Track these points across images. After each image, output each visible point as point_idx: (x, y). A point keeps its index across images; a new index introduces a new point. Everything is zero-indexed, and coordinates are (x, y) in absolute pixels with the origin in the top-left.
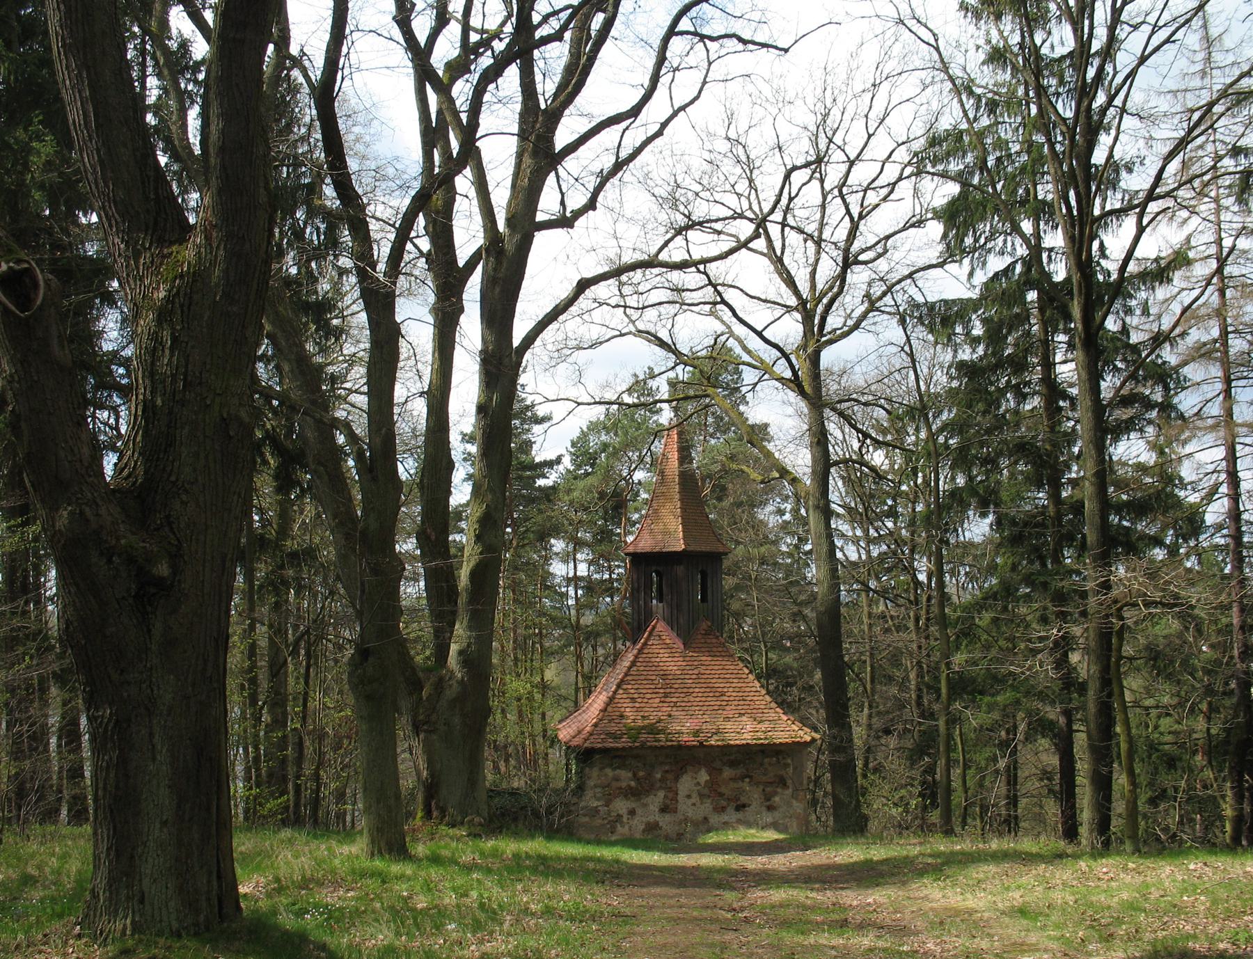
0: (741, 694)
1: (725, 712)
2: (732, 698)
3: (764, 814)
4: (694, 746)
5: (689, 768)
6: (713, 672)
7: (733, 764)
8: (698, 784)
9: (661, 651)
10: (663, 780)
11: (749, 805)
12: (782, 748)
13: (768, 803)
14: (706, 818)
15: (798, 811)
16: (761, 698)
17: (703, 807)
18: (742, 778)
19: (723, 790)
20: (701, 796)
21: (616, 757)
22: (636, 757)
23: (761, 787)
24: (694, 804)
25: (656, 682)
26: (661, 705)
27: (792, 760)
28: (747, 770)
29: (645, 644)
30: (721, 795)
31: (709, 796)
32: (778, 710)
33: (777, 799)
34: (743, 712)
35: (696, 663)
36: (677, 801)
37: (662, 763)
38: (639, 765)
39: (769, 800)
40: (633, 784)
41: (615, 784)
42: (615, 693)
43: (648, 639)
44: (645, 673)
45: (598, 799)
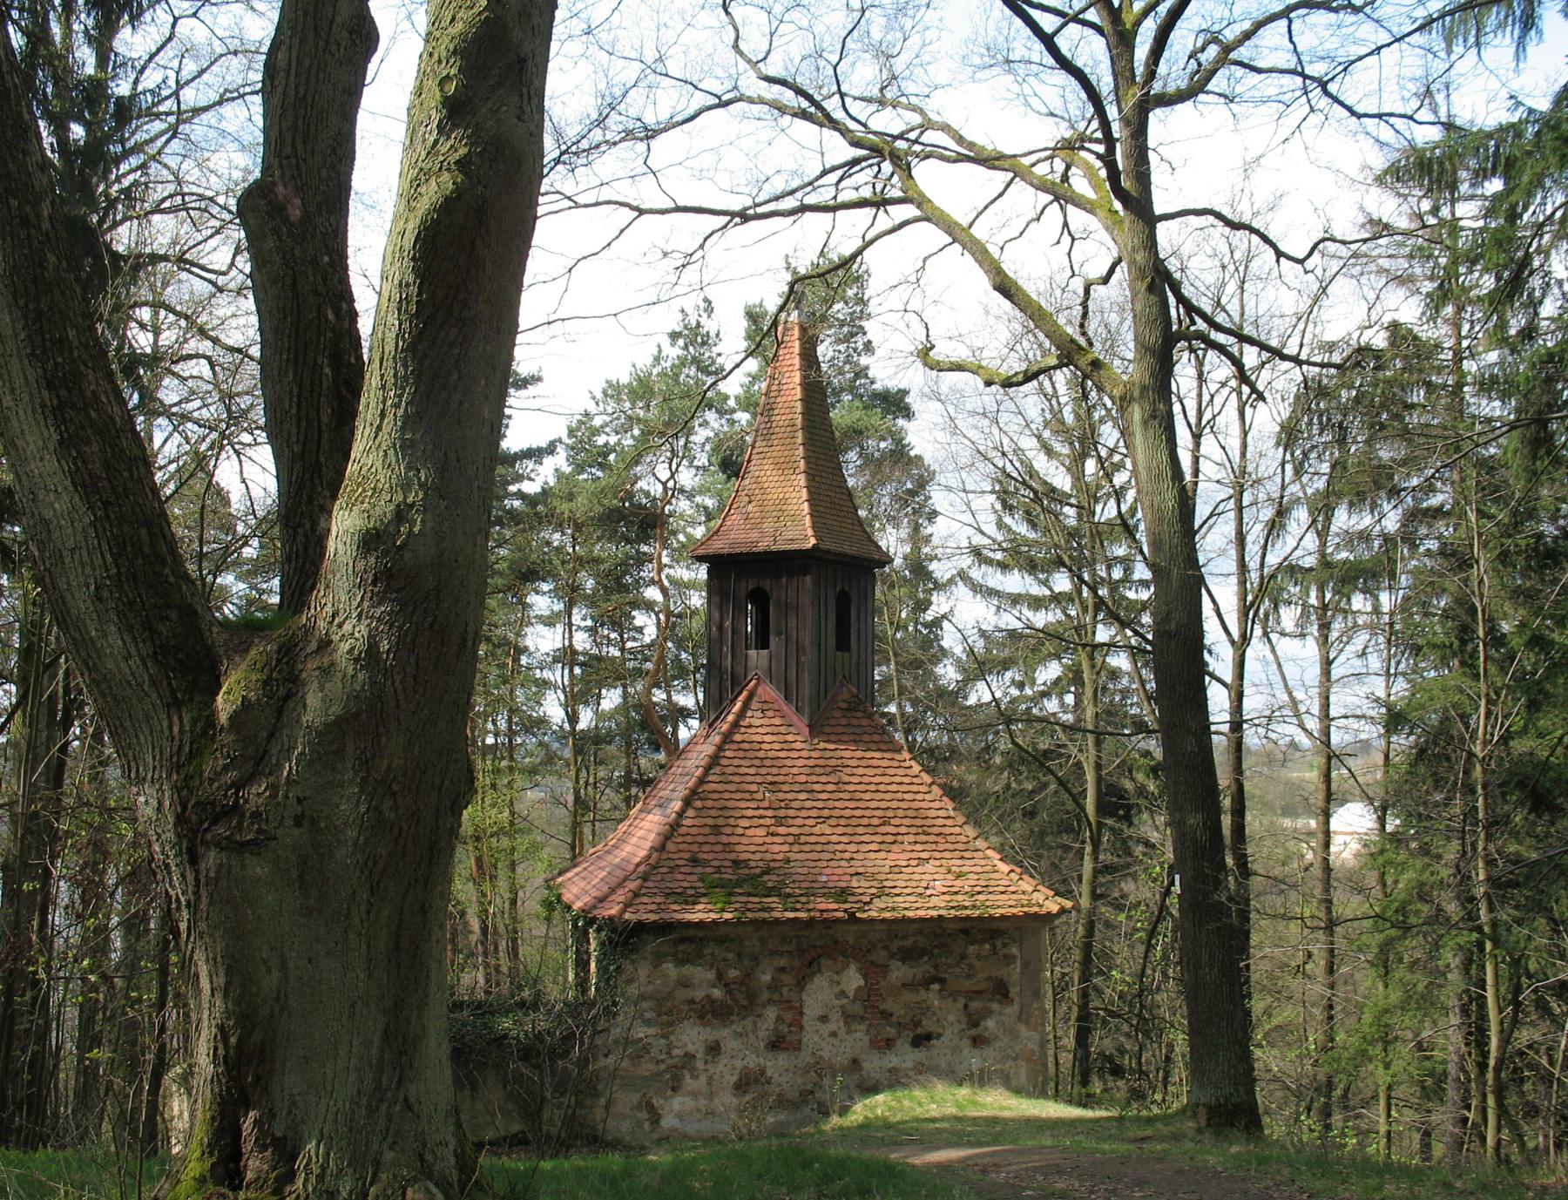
0: (919, 822)
1: (891, 856)
2: (903, 830)
3: (966, 1052)
4: (838, 921)
6: (866, 779)
7: (907, 956)
8: (843, 994)
9: (768, 738)
10: (774, 987)
11: (939, 1036)
12: (1003, 925)
13: (973, 1032)
15: (1030, 1045)
16: (958, 830)
18: (926, 983)
19: (889, 1005)
20: (848, 1018)
21: (682, 940)
22: (722, 941)
23: (962, 1001)
24: (834, 1034)
25: (759, 796)
26: (769, 839)
28: (936, 967)
29: (736, 725)
30: (887, 1015)
33: (990, 1023)
34: (925, 855)
35: (833, 762)
36: (802, 1027)
38: (730, 956)
39: (975, 1025)
40: (717, 993)
41: (681, 994)
42: (680, 814)
43: (741, 715)
44: (737, 779)
45: (648, 1023)
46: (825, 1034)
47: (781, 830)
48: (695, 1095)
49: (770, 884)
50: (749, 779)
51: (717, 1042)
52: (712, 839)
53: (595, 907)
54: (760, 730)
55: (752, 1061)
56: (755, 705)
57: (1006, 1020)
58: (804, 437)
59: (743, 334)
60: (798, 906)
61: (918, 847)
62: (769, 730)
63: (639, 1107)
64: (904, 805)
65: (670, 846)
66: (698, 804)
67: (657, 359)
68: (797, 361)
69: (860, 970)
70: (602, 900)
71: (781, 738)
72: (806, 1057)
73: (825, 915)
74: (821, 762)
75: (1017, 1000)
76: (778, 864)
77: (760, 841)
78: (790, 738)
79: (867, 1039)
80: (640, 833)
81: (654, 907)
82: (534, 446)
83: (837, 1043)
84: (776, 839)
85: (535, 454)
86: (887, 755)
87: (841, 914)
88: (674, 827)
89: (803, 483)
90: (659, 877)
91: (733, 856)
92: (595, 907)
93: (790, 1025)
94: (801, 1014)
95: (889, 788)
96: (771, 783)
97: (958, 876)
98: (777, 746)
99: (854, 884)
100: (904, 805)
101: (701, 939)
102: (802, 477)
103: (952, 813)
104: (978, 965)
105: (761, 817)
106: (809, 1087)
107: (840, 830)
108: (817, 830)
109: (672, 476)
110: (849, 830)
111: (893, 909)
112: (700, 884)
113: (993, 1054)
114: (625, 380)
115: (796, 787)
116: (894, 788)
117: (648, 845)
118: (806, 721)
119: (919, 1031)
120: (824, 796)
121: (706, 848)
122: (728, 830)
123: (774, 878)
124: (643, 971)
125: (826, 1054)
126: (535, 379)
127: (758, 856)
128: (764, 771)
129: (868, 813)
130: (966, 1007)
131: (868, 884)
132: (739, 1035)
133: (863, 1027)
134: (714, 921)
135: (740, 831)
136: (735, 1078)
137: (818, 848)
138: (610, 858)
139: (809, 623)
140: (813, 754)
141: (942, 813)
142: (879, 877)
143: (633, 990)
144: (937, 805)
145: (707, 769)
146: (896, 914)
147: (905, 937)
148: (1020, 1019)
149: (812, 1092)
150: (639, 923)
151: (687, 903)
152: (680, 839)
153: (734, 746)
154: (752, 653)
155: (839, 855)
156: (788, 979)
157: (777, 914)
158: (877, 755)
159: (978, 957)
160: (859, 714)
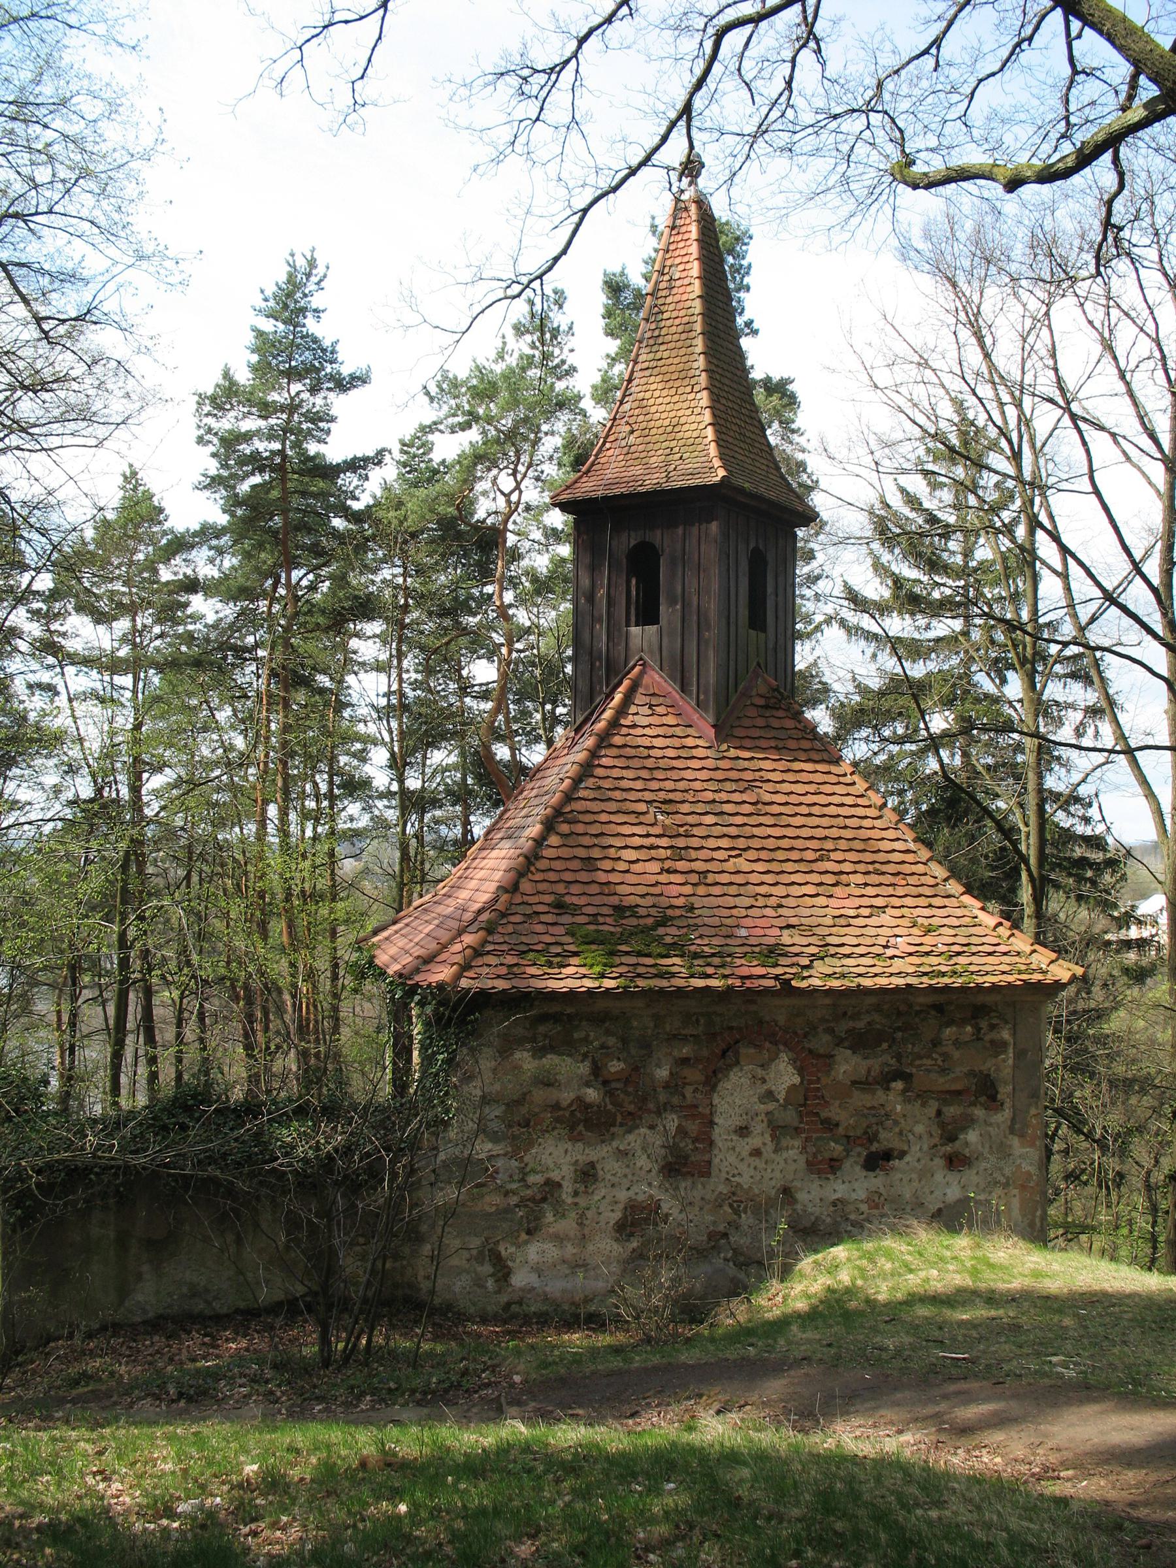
0: (868, 857)
1: (833, 902)
2: (847, 867)
3: (939, 1177)
4: (767, 991)
5: (746, 1051)
6: (793, 799)
7: (861, 1042)
8: (770, 1095)
9: (658, 742)
10: (674, 1085)
11: (902, 1154)
12: (989, 999)
13: (948, 1149)
14: (786, 1191)
15: (1026, 1167)
16: (920, 868)
17: (778, 1158)
18: (885, 1080)
19: (834, 1112)
20: (777, 1130)
21: (543, 1018)
22: (599, 1019)
23: (933, 1106)
24: (756, 1153)
25: (649, 818)
26: (663, 878)
27: (1014, 1034)
28: (899, 1057)
29: (614, 724)
30: (830, 1125)
31: (797, 1131)
32: (967, 899)
33: (972, 1136)
34: (879, 902)
35: (748, 776)
36: (711, 1143)
37: (674, 1038)
38: (611, 1041)
39: (952, 1138)
40: (592, 1094)
41: (539, 1096)
42: (539, 842)
43: (622, 711)
44: (618, 795)
45: (495, 1138)
46: (745, 1154)
47: (681, 865)
48: (559, 1239)
49: (668, 940)
50: (633, 796)
51: (592, 1165)
52: (584, 876)
53: (417, 970)
54: (647, 731)
55: (643, 1192)
56: (639, 699)
57: (993, 1131)
58: (706, 345)
59: (602, 311)
60: (710, 970)
61: (870, 891)
62: (660, 731)
63: (480, 1258)
64: (848, 834)
65: (525, 886)
66: (565, 828)
67: (501, 356)
68: (694, 249)
69: (793, 1062)
70: (428, 960)
71: (676, 742)
72: (717, 1185)
73: (748, 984)
74: (734, 775)
75: (1008, 1104)
76: (678, 912)
77: (652, 879)
78: (690, 742)
79: (802, 1160)
80: (481, 874)
81: (503, 970)
82: (359, 455)
83: (761, 1165)
84: (674, 878)
85: (356, 465)
86: (819, 767)
87: (770, 983)
88: (530, 860)
89: (705, 402)
90: (510, 928)
91: (614, 900)
92: (417, 970)
93: (696, 1140)
94: (712, 1123)
95: (826, 810)
96: (665, 802)
97: (928, 931)
98: (671, 753)
99: (786, 940)
100: (848, 834)
101: (570, 1017)
102: (705, 394)
103: (912, 846)
104: (956, 1054)
105: (652, 847)
106: (721, 1228)
107: (760, 867)
108: (729, 866)
109: (518, 487)
110: (775, 867)
111: (843, 976)
112: (568, 939)
113: (975, 1179)
114: (462, 375)
115: (700, 808)
116: (832, 810)
117: (492, 887)
118: (711, 720)
119: (875, 1147)
120: (739, 820)
121: (575, 889)
122: (607, 865)
123: (673, 931)
124: (486, 1063)
125: (745, 1181)
126: (358, 380)
127: (648, 901)
128: (655, 785)
129: (799, 844)
130: (939, 1113)
131: (805, 941)
132: (623, 1154)
133: (797, 1143)
134: (590, 992)
135: (622, 866)
136: (618, 1215)
137: (733, 890)
138: (440, 909)
139: (715, 586)
140: (721, 764)
141: (898, 845)
142: (819, 931)
143: (475, 1090)
144: (891, 834)
145: (577, 781)
146: (847, 983)
147: (855, 1017)
148: (1012, 1130)
149: (725, 1235)
150: (483, 994)
151: (550, 964)
152: (538, 877)
153: (614, 752)
154: (635, 630)
155: (761, 902)
156: (694, 1075)
157: (680, 983)
158: (809, 766)
159: (957, 1043)
160: (780, 713)
